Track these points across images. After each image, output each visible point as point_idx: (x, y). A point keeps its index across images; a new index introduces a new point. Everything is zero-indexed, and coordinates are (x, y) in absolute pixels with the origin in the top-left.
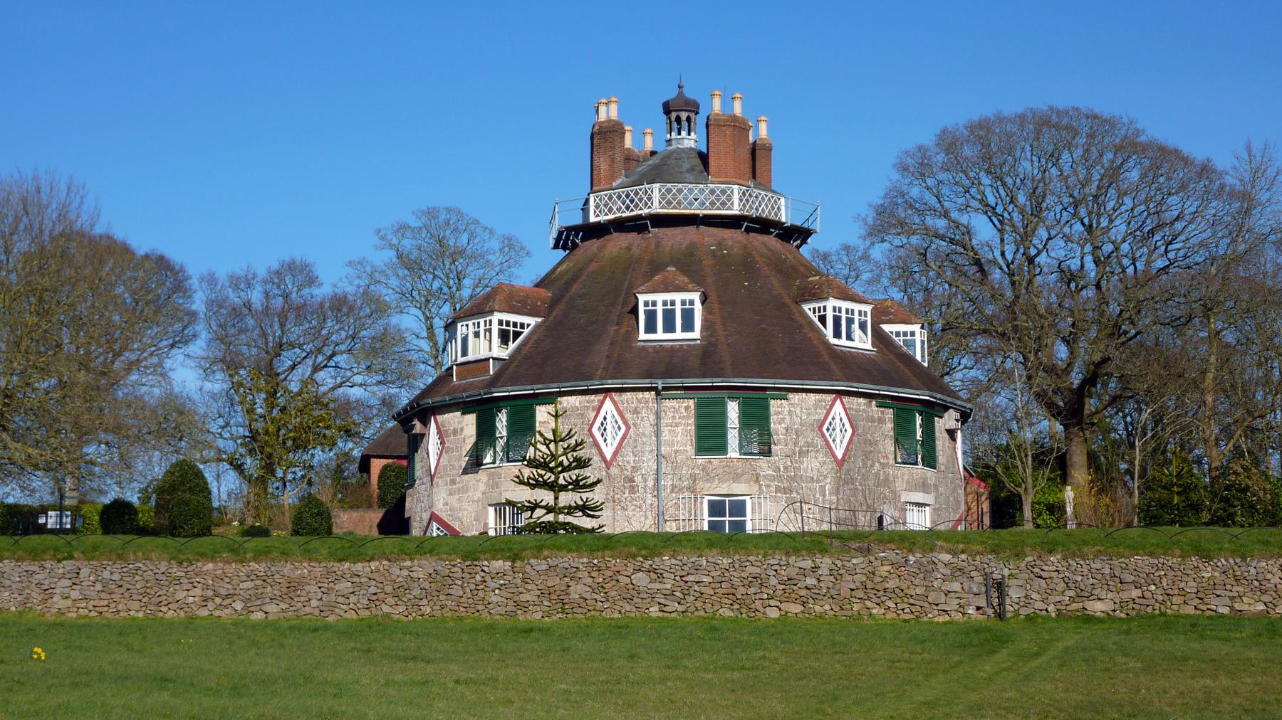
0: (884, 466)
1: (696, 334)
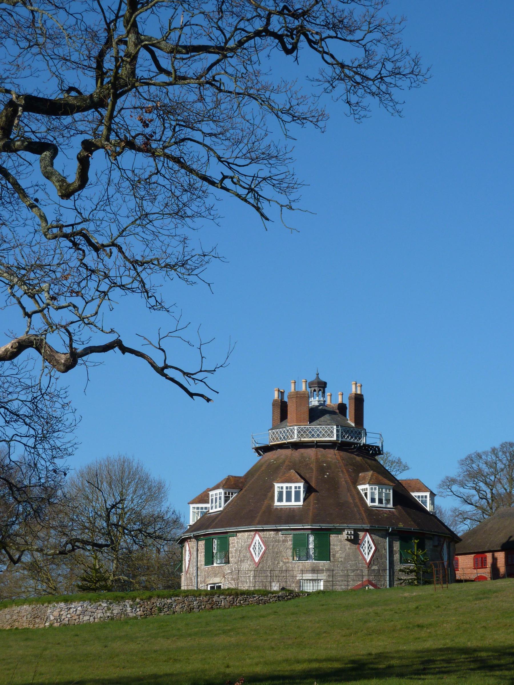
0: (285, 563)
1: (301, 503)
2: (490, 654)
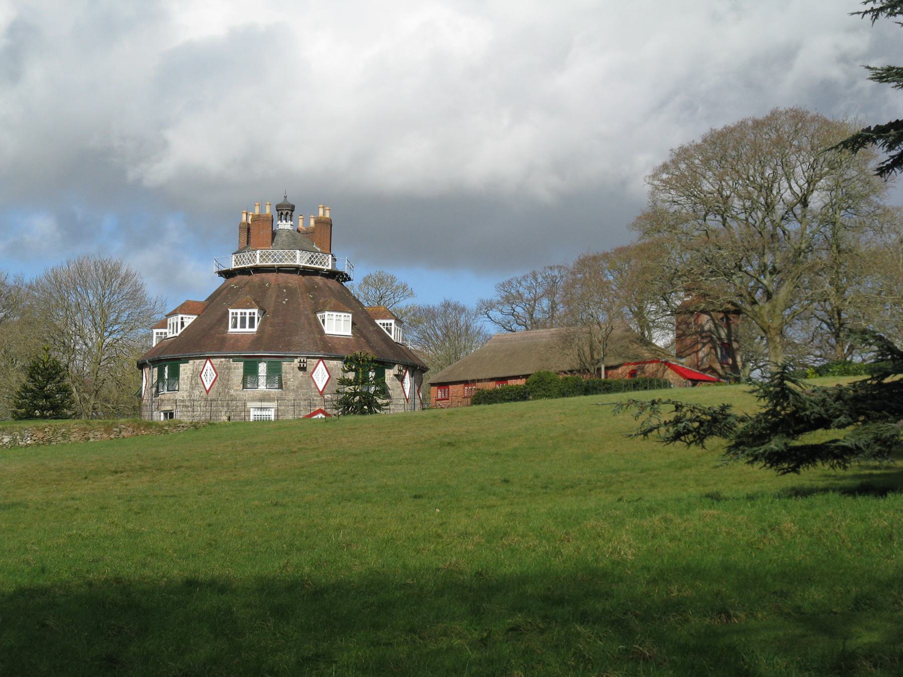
1: (255, 330)
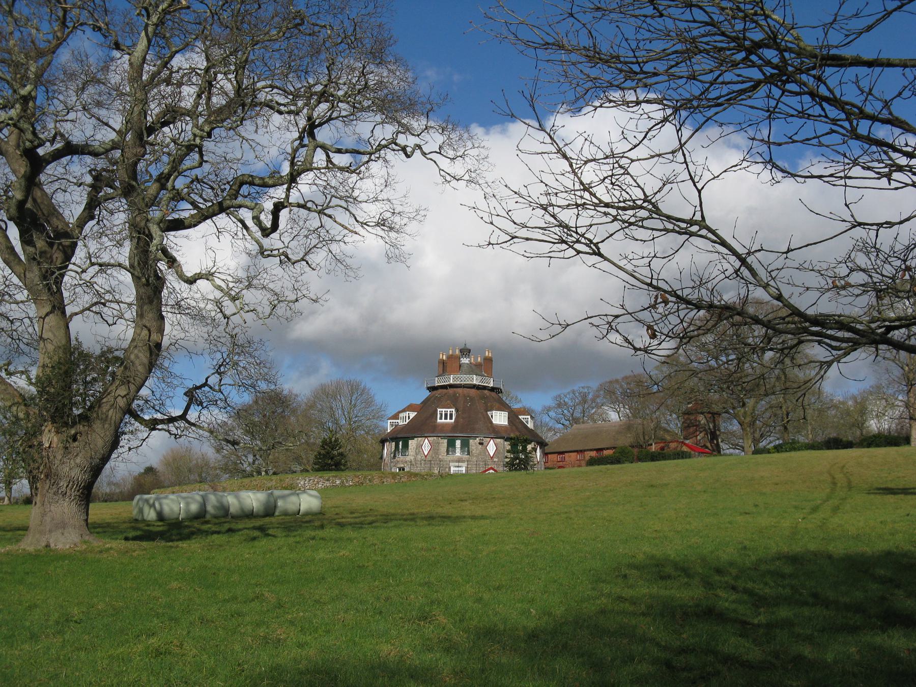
2: (829, 332)
